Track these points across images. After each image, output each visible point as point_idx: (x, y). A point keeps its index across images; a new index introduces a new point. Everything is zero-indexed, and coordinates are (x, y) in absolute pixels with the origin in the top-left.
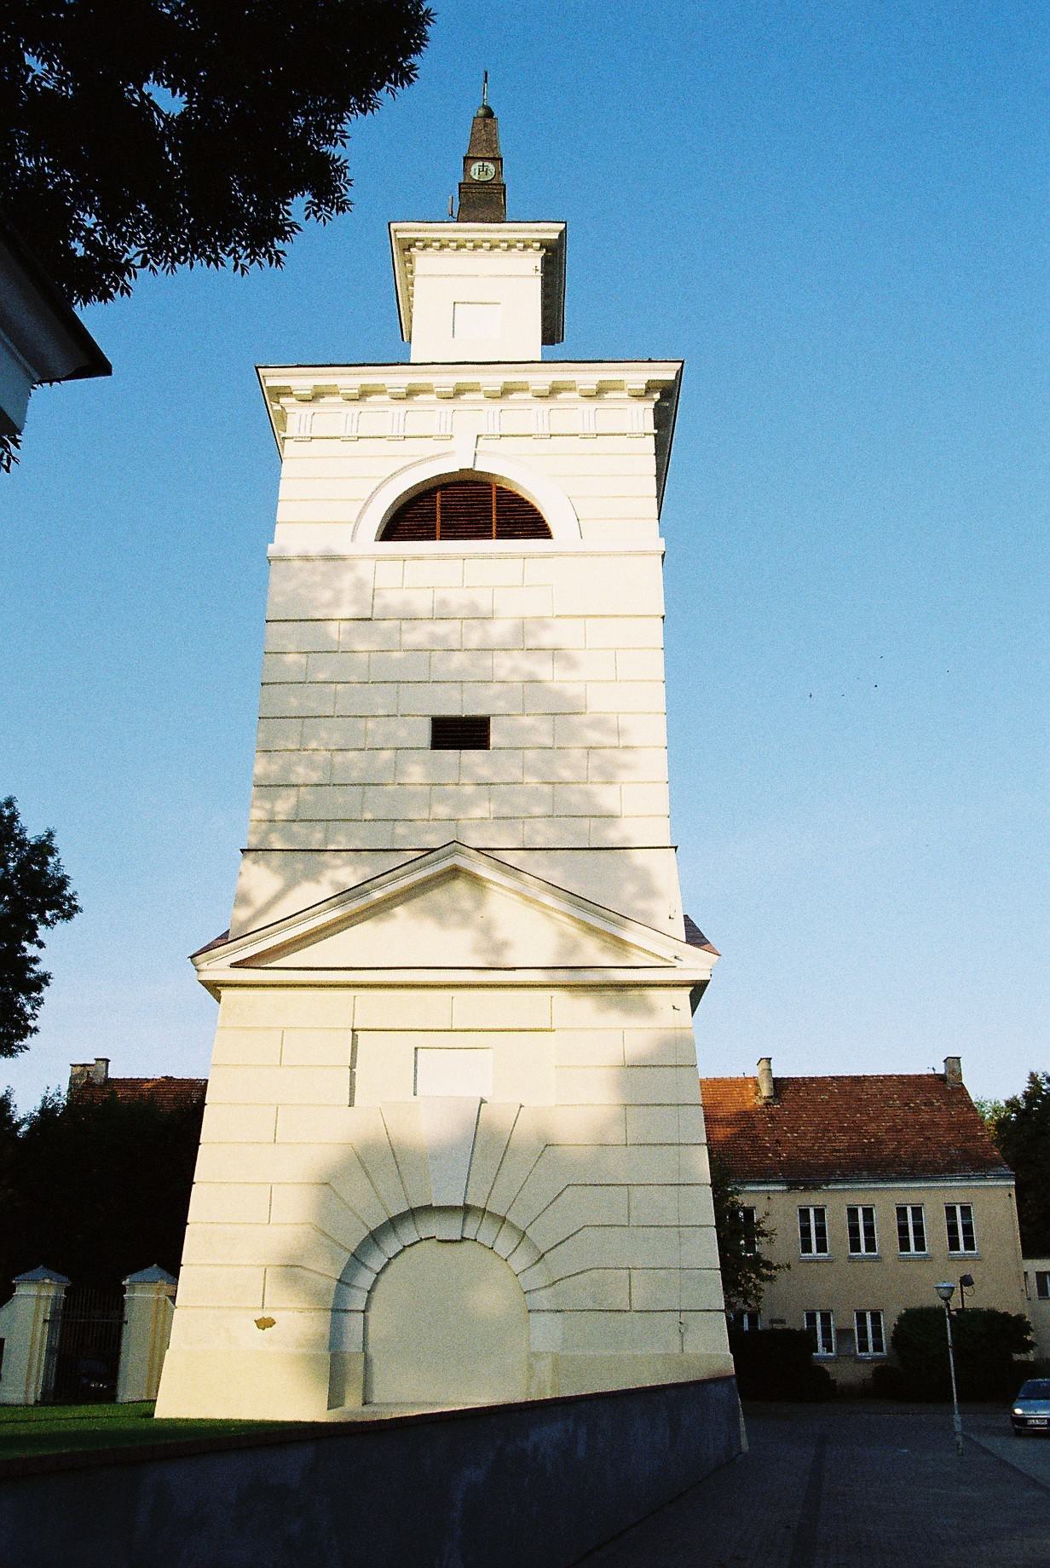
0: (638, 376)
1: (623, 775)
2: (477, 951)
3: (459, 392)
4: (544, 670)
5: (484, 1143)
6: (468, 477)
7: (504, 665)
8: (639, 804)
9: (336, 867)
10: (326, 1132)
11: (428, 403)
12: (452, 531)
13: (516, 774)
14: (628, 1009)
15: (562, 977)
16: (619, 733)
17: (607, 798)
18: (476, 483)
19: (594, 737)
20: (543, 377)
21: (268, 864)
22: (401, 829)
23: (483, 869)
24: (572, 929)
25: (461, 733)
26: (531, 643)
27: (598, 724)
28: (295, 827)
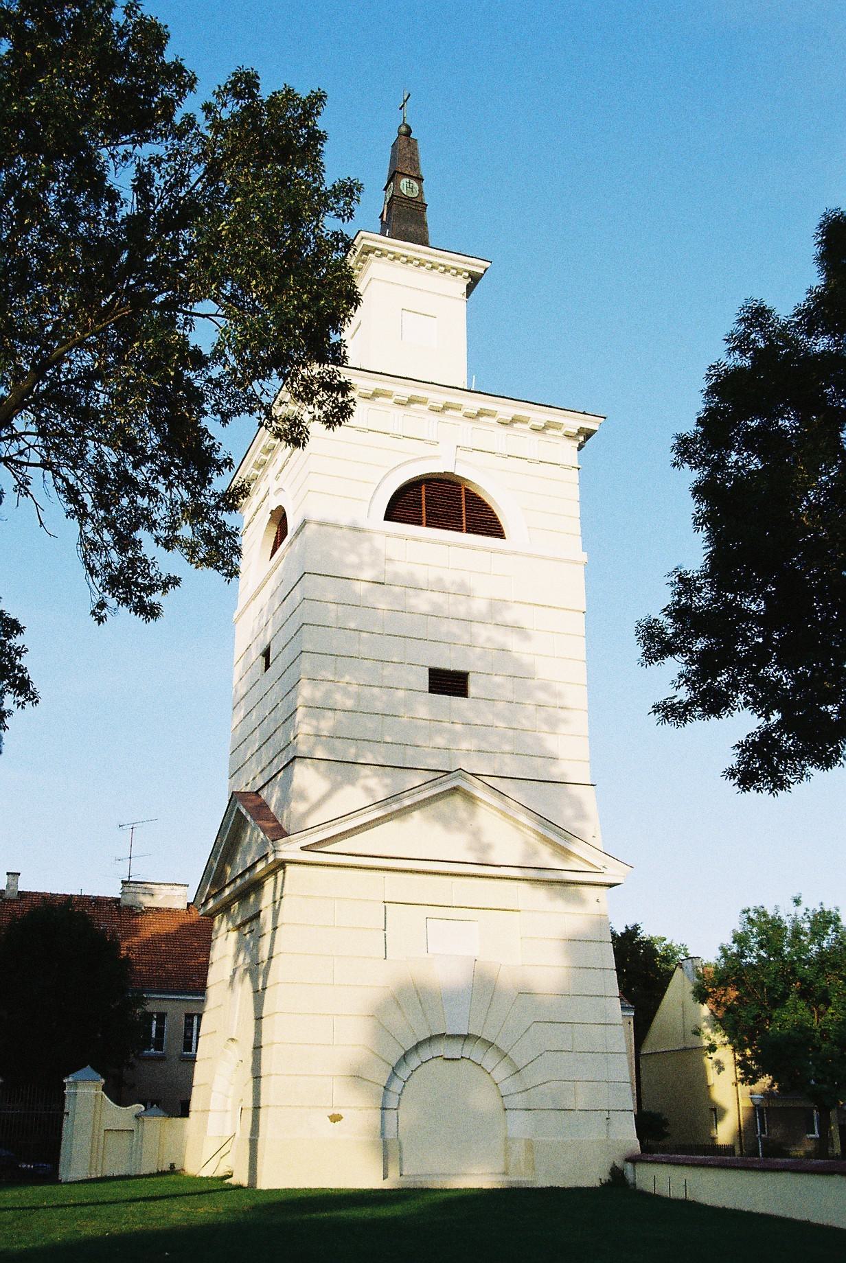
0: (574, 423)
1: (562, 729)
2: (470, 849)
3: (411, 401)
4: (512, 642)
5: (484, 988)
6: (452, 479)
7: (484, 634)
8: (571, 751)
9: (367, 777)
10: (375, 979)
11: (456, 418)
12: (435, 521)
13: (489, 719)
14: (569, 899)
15: (532, 874)
16: (559, 695)
17: (552, 743)
18: (450, 482)
19: (542, 697)
20: (474, 403)
21: (317, 769)
22: (410, 751)
23: (479, 792)
24: (533, 838)
25: (448, 683)
26: (499, 619)
27: (545, 687)
28: (338, 742)
